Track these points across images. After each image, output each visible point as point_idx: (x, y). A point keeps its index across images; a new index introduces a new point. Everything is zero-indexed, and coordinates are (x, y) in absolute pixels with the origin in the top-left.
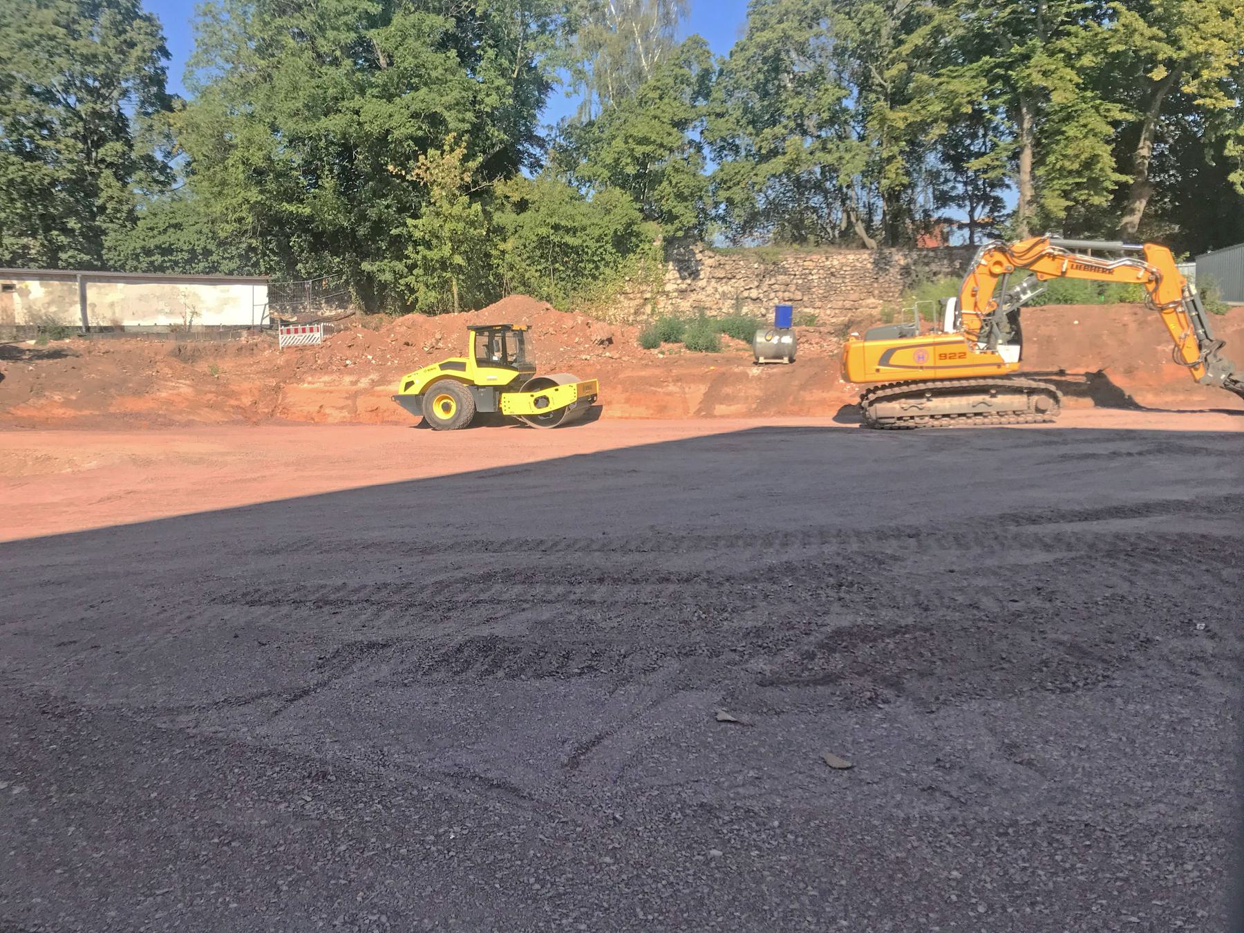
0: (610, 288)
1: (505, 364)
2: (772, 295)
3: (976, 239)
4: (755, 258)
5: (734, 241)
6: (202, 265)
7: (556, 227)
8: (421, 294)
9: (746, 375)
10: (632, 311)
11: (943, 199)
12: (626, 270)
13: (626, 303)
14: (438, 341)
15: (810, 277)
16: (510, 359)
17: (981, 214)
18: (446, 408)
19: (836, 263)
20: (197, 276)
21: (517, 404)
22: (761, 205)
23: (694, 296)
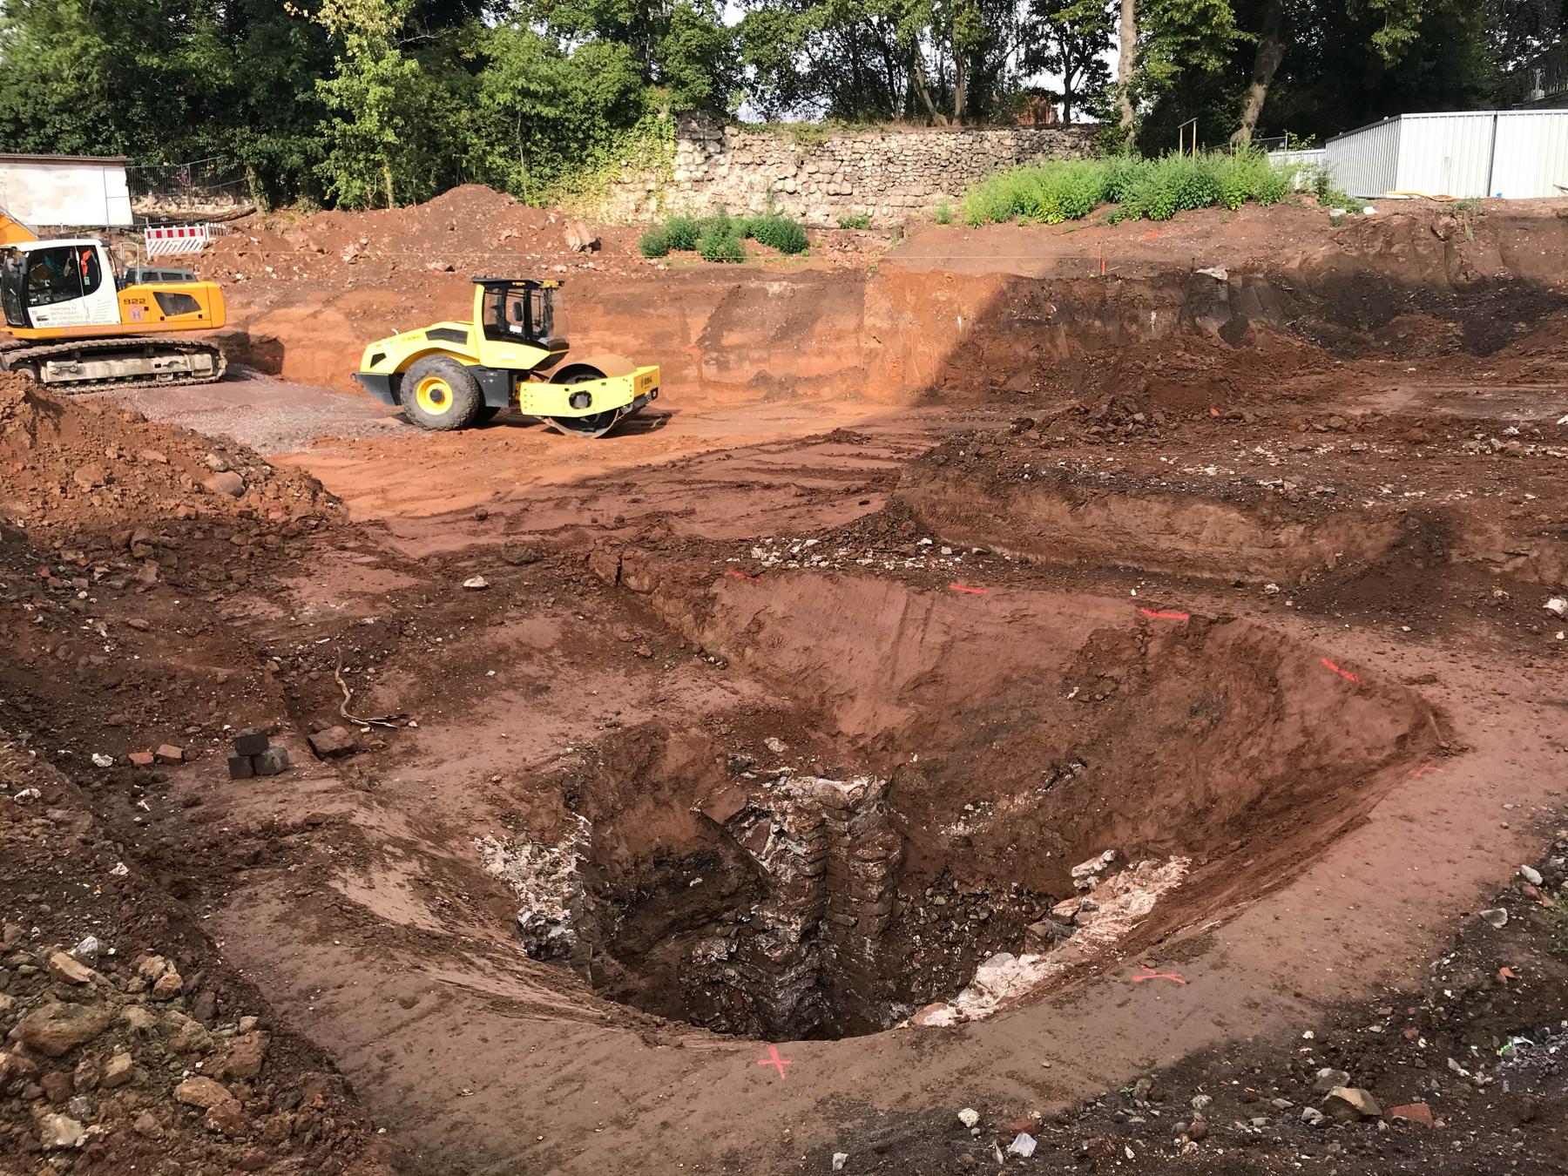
0: (602, 176)
1: (529, 338)
2: (813, 188)
3: (1072, 116)
4: (791, 136)
5: (768, 117)
6: (31, 139)
7: (525, 93)
8: (341, 183)
9: (766, 293)
10: (633, 207)
11: (1035, 62)
12: (622, 151)
13: (623, 196)
14: (364, 247)
15: (862, 164)
16: (536, 330)
17: (1079, 82)
18: (437, 397)
19: (894, 145)
20: (26, 156)
21: (542, 399)
22: (803, 67)
23: (711, 188)
